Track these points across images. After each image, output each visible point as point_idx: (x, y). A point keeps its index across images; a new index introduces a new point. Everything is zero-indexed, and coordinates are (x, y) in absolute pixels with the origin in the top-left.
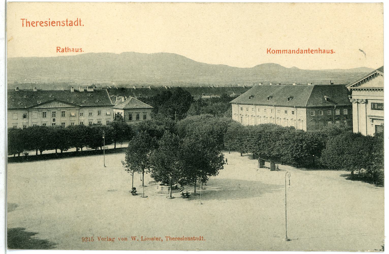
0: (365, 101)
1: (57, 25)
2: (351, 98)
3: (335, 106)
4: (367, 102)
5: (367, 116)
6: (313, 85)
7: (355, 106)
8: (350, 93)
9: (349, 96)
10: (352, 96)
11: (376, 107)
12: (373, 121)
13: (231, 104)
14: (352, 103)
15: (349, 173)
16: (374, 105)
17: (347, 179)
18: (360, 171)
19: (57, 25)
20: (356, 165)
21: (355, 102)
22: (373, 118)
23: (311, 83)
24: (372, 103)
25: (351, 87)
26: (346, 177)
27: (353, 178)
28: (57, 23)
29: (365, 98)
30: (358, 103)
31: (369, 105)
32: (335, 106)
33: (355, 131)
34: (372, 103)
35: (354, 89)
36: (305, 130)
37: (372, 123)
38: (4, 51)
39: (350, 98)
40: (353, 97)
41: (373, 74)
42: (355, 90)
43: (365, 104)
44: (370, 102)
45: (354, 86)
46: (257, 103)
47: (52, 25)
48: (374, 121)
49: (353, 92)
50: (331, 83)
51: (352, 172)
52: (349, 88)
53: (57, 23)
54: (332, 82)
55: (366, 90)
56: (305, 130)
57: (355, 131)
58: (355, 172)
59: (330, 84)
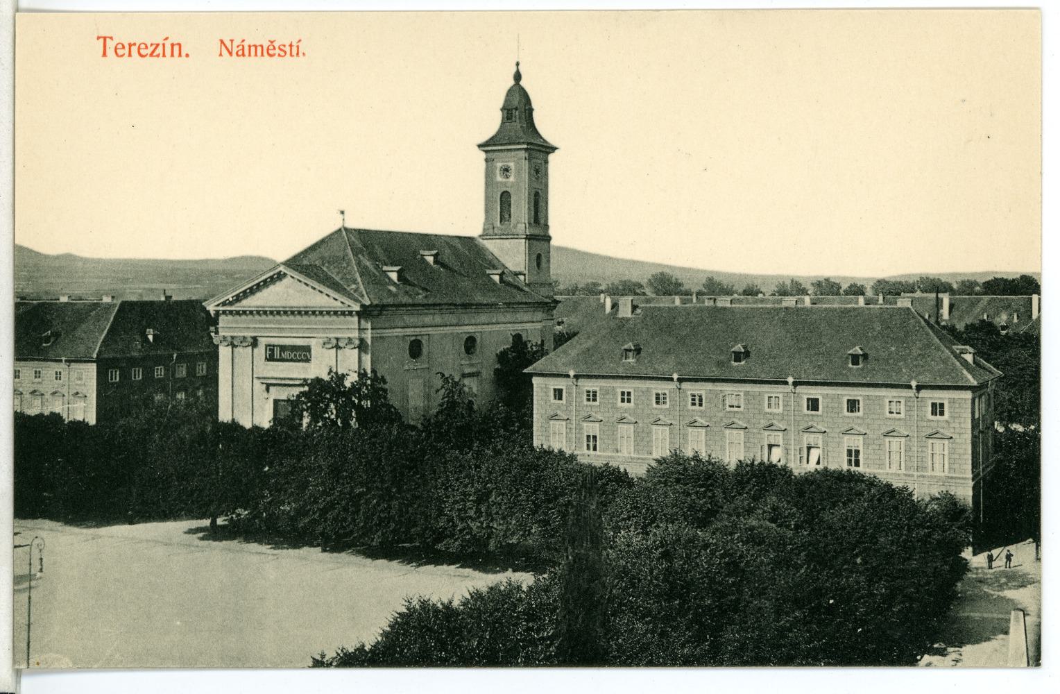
0: (250, 340)
1: (130, 55)
2: (217, 333)
3: (175, 356)
4: (254, 343)
5: (255, 380)
6: (118, 302)
7: (224, 352)
8: (213, 321)
9: (212, 329)
10: (220, 330)
11: (277, 355)
12: (268, 390)
13: (531, 375)
14: (218, 346)
15: (206, 523)
16: (272, 350)
17: (202, 539)
18: (234, 516)
19: (130, 55)
20: (228, 502)
21: (226, 344)
22: (269, 382)
23: (113, 297)
24: (267, 346)
25: (218, 305)
26: (201, 535)
27: (215, 533)
28: (130, 49)
29: (249, 334)
30: (234, 346)
31: (260, 351)
32: (175, 356)
33: (224, 416)
34: (267, 346)
35: (224, 312)
36: (92, 420)
37: (265, 394)
38: (1043, 154)
39: (213, 334)
40: (222, 333)
41: (271, 274)
42: (227, 315)
43: (335, 349)
44: (263, 342)
45: (224, 304)
46: (763, 376)
47: (269, 54)
48: (272, 389)
49: (222, 318)
50: (166, 297)
51: (214, 522)
52: (211, 308)
53: (130, 49)
54: (168, 294)
55: (317, 313)
56: (92, 420)
57: (224, 416)
58: (220, 521)
59: (163, 299)
